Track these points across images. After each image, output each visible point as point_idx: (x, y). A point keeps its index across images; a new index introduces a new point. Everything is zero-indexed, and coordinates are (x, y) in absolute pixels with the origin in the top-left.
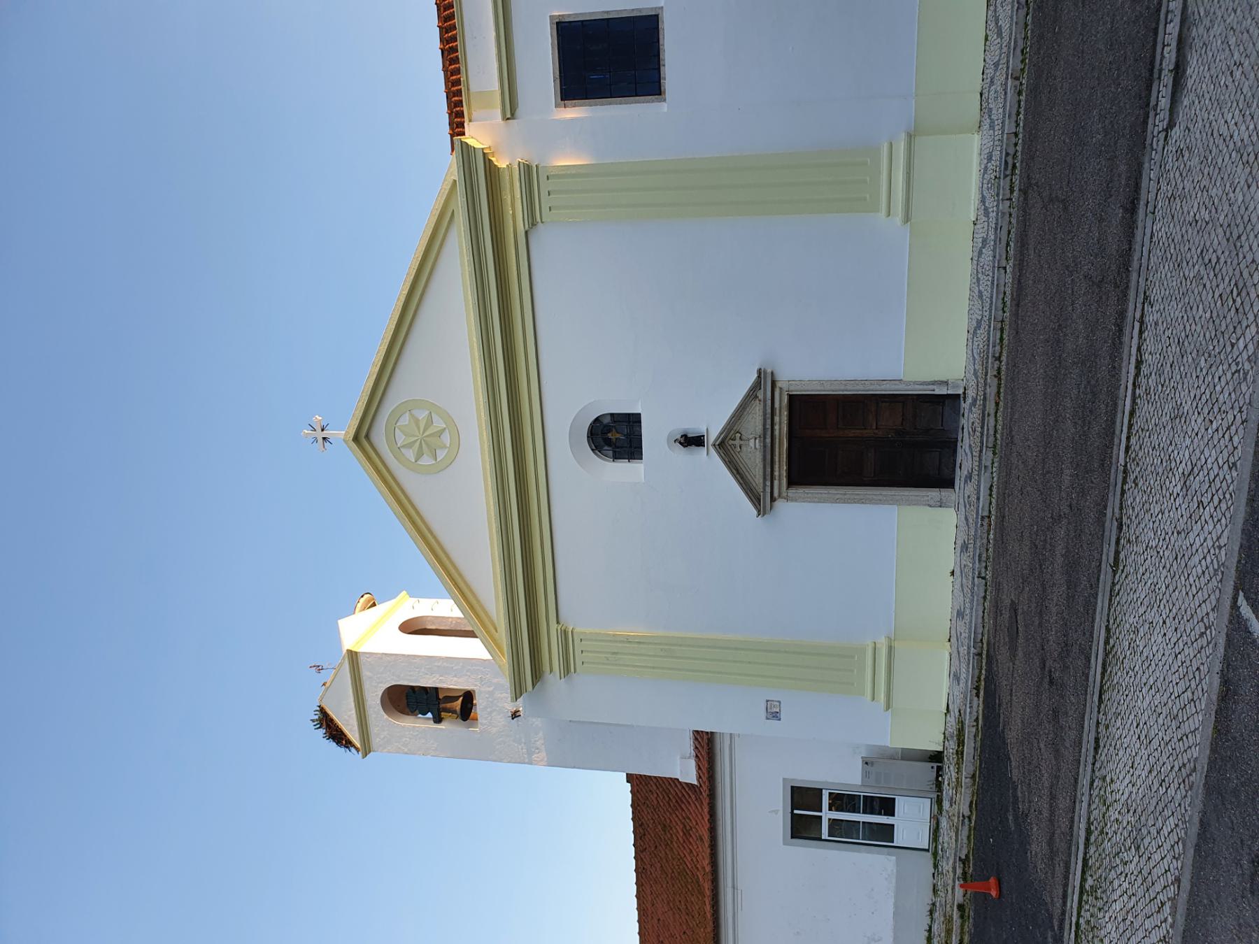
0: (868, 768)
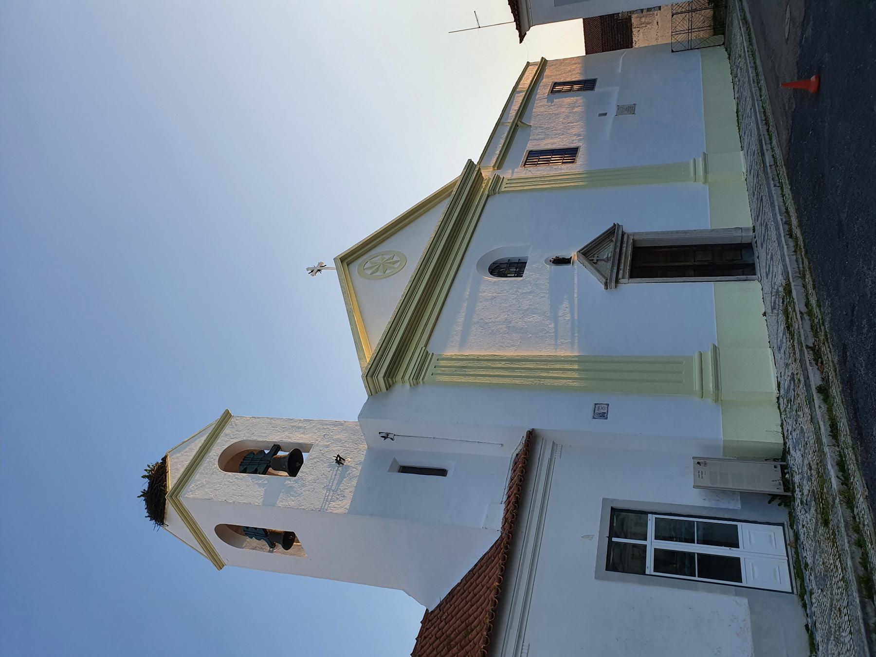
0: (701, 468)
